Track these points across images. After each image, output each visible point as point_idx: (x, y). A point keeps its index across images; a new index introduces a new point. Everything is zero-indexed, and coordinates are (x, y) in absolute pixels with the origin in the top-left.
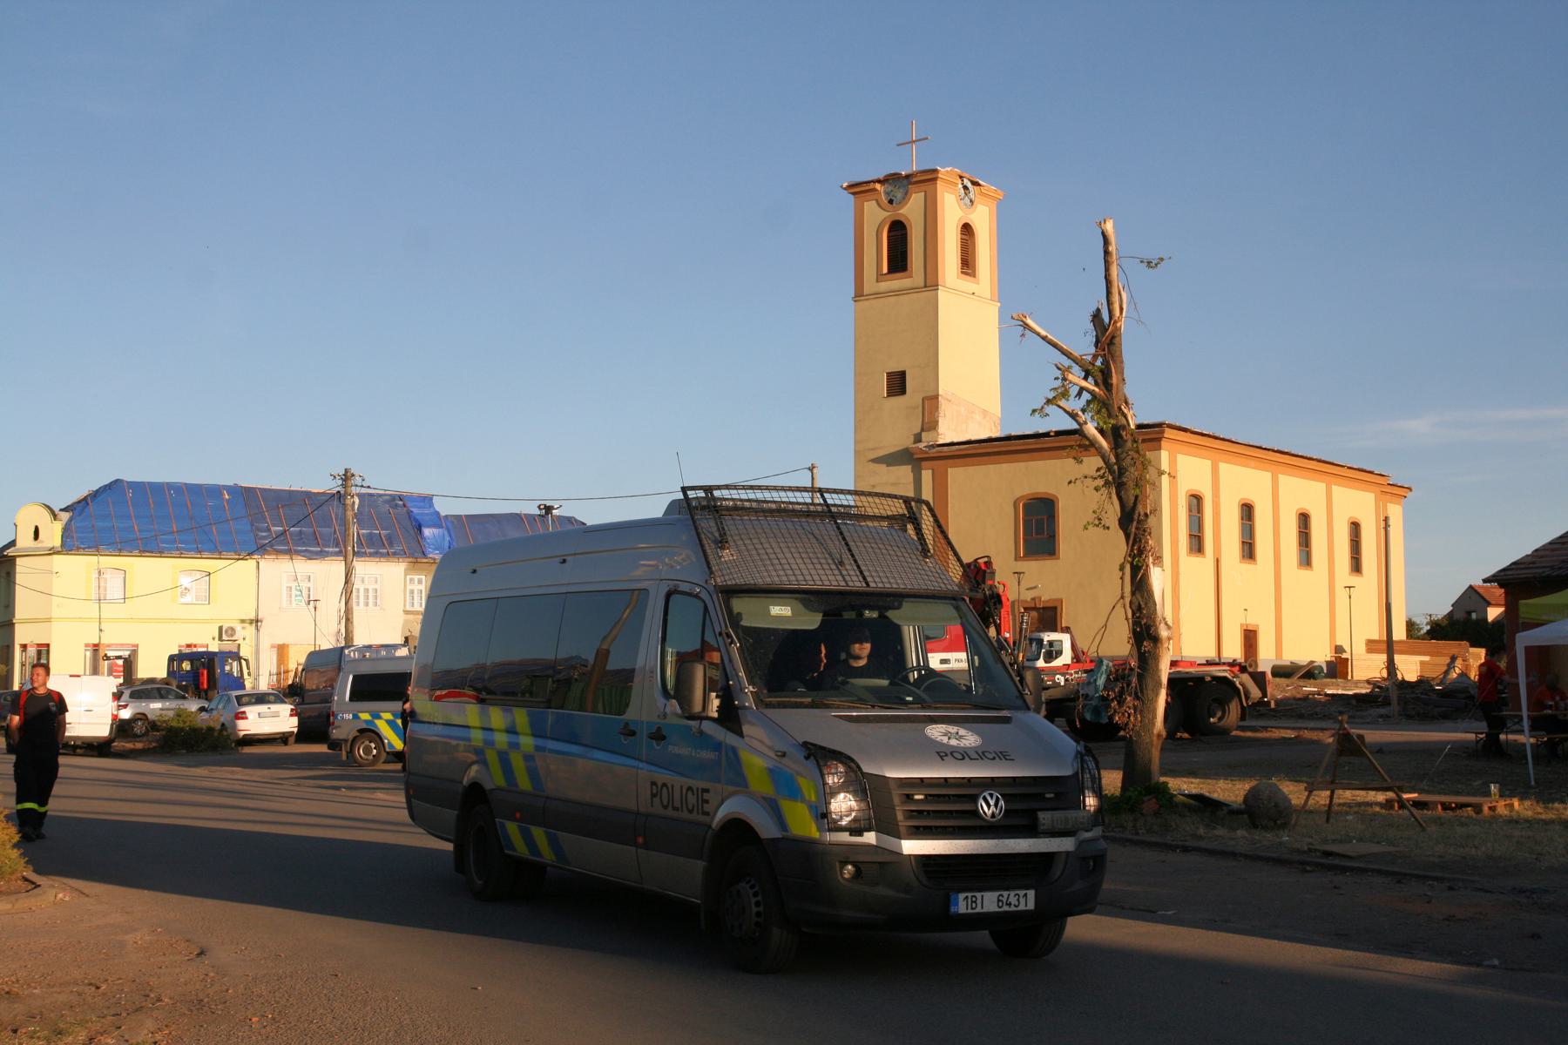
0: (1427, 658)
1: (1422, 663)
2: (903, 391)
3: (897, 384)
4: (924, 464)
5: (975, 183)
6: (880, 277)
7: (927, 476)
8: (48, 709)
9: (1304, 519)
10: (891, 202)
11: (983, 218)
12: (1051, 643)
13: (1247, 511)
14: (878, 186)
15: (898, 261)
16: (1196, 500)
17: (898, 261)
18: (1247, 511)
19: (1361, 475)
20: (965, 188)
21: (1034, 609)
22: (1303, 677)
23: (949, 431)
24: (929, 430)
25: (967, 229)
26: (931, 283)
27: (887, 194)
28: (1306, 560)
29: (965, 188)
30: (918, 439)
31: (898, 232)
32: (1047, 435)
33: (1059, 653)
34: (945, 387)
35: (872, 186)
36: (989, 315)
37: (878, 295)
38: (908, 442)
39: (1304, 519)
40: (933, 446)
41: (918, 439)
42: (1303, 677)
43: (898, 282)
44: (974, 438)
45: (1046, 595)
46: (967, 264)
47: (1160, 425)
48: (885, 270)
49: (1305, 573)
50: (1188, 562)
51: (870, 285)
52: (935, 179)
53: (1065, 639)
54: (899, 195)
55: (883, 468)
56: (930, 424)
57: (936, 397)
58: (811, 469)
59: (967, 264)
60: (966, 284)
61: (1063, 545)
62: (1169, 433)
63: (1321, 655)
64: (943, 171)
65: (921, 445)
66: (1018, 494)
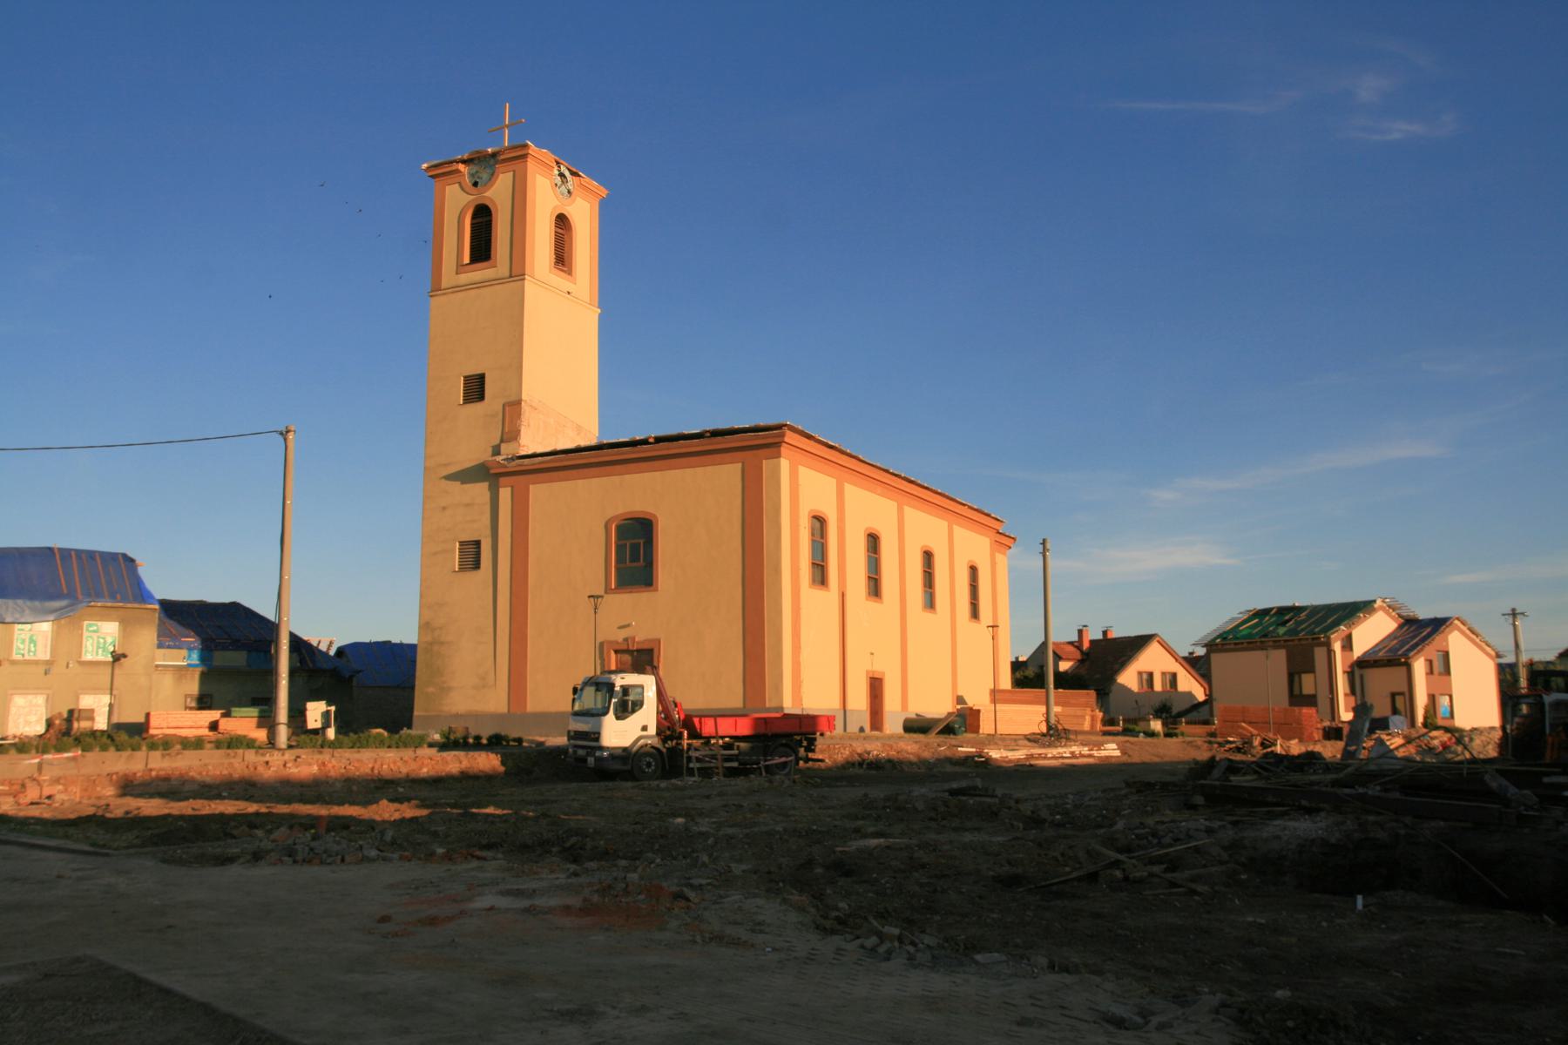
2: (481, 397)
3: (475, 388)
4: (502, 480)
5: (573, 174)
6: (460, 269)
7: (505, 494)
9: (928, 556)
10: (475, 184)
11: (584, 215)
12: (626, 690)
13: (873, 541)
14: (461, 167)
15: (481, 250)
16: (819, 521)
17: (481, 250)
18: (873, 541)
19: (980, 518)
20: (562, 175)
21: (627, 651)
22: (942, 732)
23: (534, 439)
24: (509, 441)
25: (562, 221)
26: (517, 274)
27: (472, 175)
28: (930, 604)
29: (562, 175)
31: (483, 217)
32: (645, 442)
33: (638, 705)
34: (531, 390)
35: (454, 167)
37: (458, 288)
38: (484, 455)
39: (928, 556)
40: (512, 459)
42: (942, 732)
43: (482, 273)
44: (560, 447)
45: (641, 634)
46: (562, 258)
47: (779, 427)
48: (467, 260)
49: (929, 615)
51: (449, 277)
52: (525, 156)
53: (648, 682)
54: (485, 176)
55: (456, 486)
56: (511, 435)
57: (519, 402)
58: (284, 434)
59: (562, 258)
62: (790, 437)
63: (938, 707)
65: (499, 458)
66: (611, 513)
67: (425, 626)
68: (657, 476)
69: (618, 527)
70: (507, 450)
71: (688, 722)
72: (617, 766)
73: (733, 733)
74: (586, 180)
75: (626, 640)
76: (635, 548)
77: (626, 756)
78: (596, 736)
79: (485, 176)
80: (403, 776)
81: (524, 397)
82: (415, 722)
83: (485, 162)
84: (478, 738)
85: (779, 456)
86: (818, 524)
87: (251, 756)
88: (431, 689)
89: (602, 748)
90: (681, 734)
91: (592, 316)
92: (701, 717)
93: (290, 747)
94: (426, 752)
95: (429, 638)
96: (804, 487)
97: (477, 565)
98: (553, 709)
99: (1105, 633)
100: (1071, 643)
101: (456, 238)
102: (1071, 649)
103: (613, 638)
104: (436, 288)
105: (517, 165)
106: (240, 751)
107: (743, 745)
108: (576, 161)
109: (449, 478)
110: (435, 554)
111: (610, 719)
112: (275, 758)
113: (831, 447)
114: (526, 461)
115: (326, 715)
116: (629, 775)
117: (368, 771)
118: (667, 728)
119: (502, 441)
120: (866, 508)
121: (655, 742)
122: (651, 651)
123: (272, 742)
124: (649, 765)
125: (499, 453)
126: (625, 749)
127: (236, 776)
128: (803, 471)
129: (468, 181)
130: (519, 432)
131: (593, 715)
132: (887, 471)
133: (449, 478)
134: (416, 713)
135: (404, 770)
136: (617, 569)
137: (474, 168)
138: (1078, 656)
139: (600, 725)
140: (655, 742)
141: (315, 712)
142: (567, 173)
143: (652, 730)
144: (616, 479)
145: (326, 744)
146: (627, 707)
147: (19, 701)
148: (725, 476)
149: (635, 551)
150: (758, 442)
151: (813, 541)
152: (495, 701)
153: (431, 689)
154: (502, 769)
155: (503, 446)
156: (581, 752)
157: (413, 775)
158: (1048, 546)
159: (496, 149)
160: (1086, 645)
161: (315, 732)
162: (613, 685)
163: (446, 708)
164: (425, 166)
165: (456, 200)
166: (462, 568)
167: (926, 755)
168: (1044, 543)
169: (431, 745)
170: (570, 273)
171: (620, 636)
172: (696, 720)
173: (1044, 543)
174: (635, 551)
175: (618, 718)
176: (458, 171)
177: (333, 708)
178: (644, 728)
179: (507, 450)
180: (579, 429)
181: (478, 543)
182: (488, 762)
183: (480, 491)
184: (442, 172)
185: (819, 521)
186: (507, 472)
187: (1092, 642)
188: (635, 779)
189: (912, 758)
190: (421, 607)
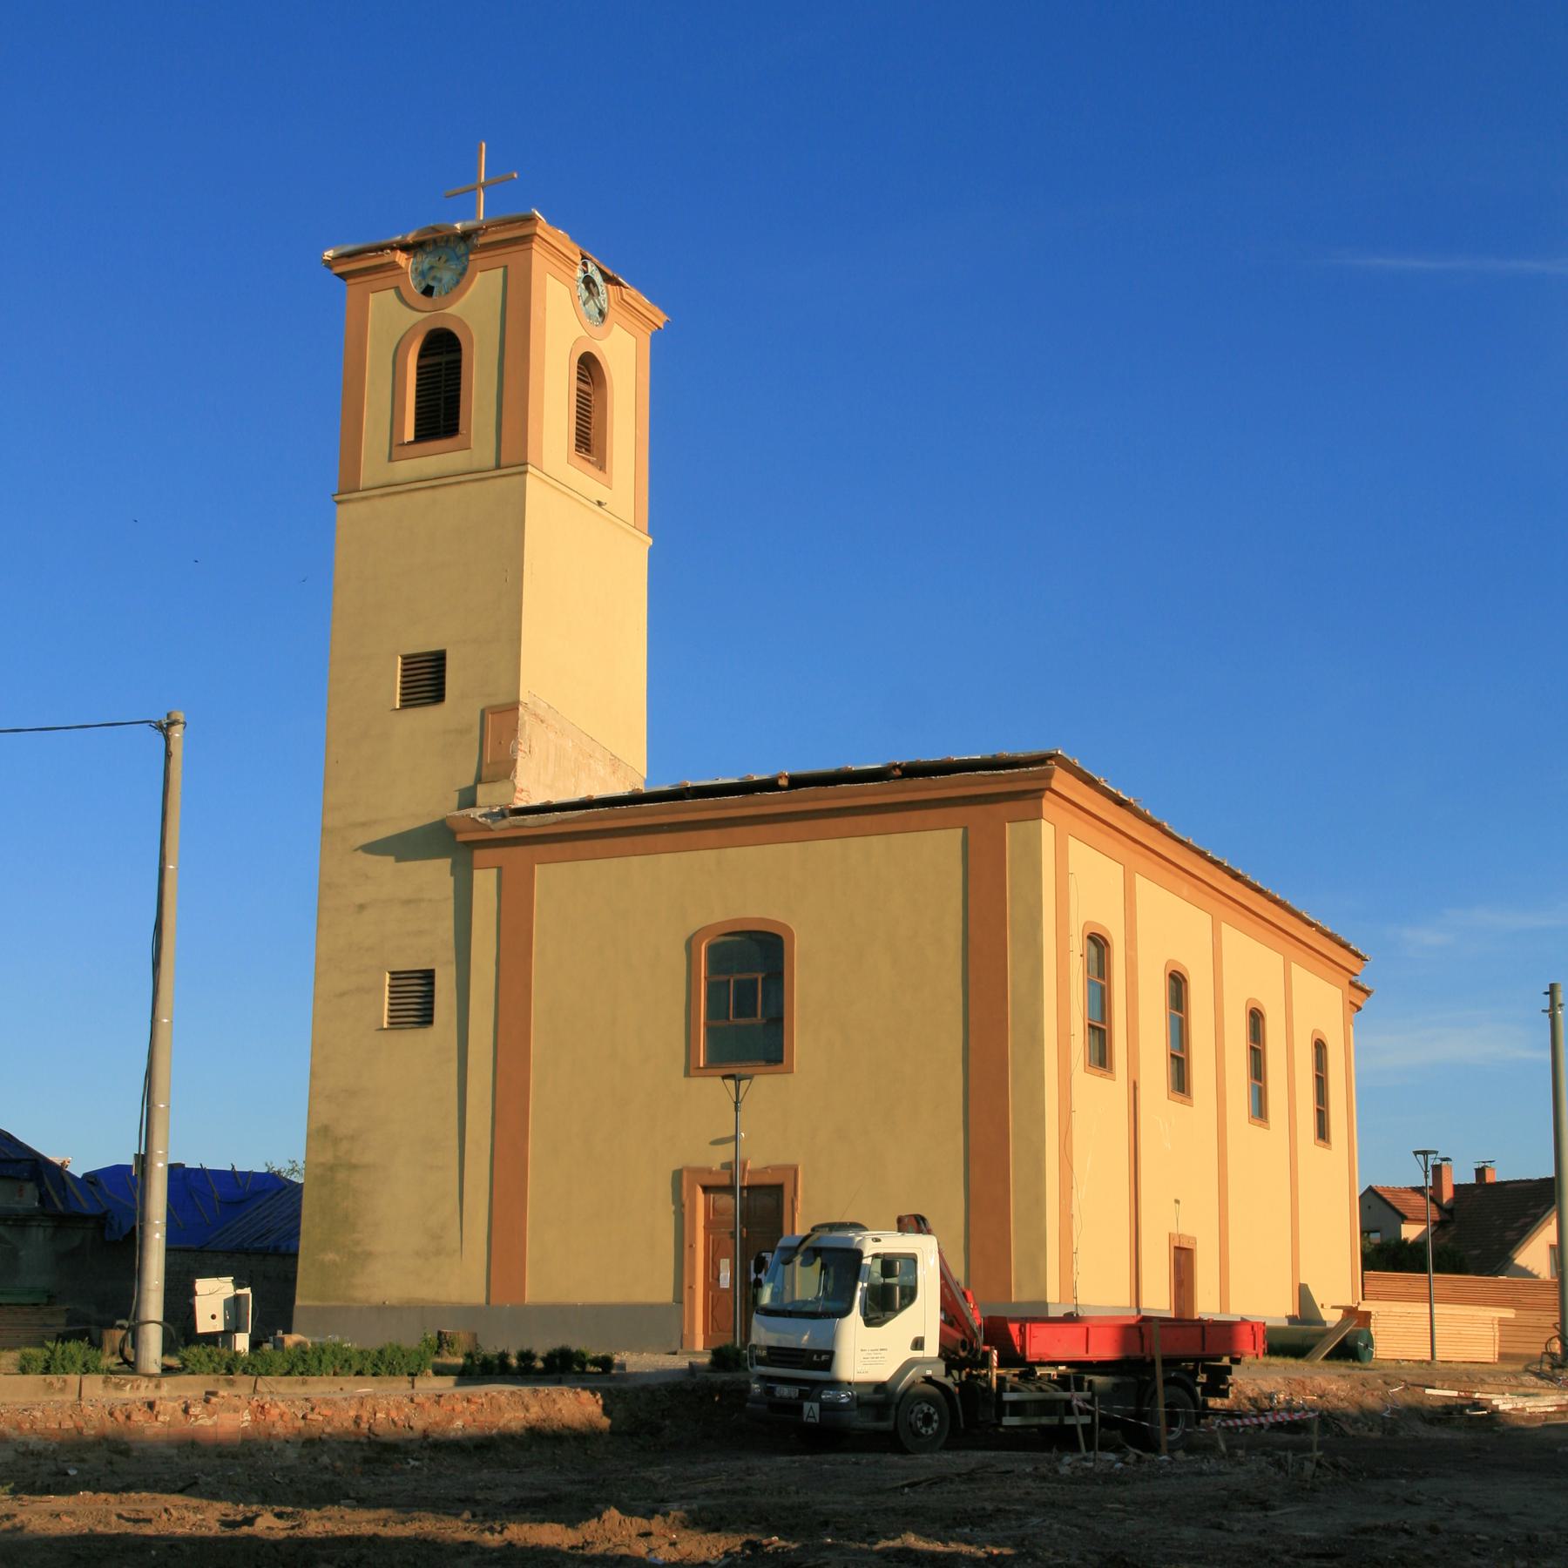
0: (1509, 1313)
1: (1503, 1323)
2: (438, 695)
3: (426, 679)
4: (479, 855)
5: (608, 279)
6: (396, 449)
7: (485, 882)
8: (748, 1389)
9: (1256, 1018)
10: (428, 291)
11: (625, 356)
12: (887, 1263)
14: (401, 258)
15: (439, 414)
16: (1098, 942)
17: (439, 414)
19: (1336, 951)
21: (729, 1189)
23: (540, 779)
25: (589, 368)
26: (511, 460)
27: (422, 275)
28: (1260, 1111)
30: (468, 799)
31: (442, 357)
32: (770, 785)
34: (537, 683)
35: (387, 256)
36: (624, 561)
37: (391, 488)
38: (445, 807)
40: (502, 815)
41: (468, 799)
43: (439, 459)
44: (598, 793)
47: (1041, 760)
48: (409, 435)
50: (1086, 1082)
51: (373, 464)
52: (527, 239)
54: (447, 277)
57: (513, 707)
58: (165, 729)
60: (580, 476)
61: (802, 1038)
62: (1062, 781)
64: (543, 227)
65: (475, 813)
66: (698, 921)
67: (320, 1134)
68: (792, 851)
69: (712, 949)
70: (491, 798)
71: (996, 1330)
72: (862, 1421)
73: (1079, 1354)
74: (631, 294)
75: (727, 1166)
76: (745, 996)
77: (880, 1397)
78: (825, 1359)
79: (447, 277)
80: (416, 1434)
81: (523, 697)
82: (298, 1318)
83: (447, 249)
84: (526, 1357)
85: (1038, 816)
86: (1094, 950)
87: (1227, 1478)
88: (330, 1256)
89: (836, 1384)
90: (986, 1355)
91: (635, 552)
92: (1023, 1321)
93: (167, 1370)
94: (430, 1384)
95: (327, 1157)
96: (1079, 876)
97: (426, 1017)
98: (579, 1297)
99: (1480, 1172)
100: (1419, 1190)
101: (388, 392)
102: (1418, 1200)
103: (699, 1162)
104: (349, 487)
105: (511, 256)
106: (73, 1379)
107: (1098, 1380)
108: (612, 264)
109: (372, 848)
110: (342, 995)
111: (853, 1322)
112: (134, 1392)
113: (1121, 803)
114: (530, 819)
115: (234, 1305)
116: (891, 1442)
117: (349, 1424)
118: (965, 1341)
119: (479, 780)
120: (1169, 925)
121: (937, 1371)
122: (777, 1189)
123: (131, 1366)
124: (927, 1420)
125: (473, 804)
126: (880, 1387)
127: (89, 1432)
128: (1078, 851)
129: (413, 285)
130: (512, 764)
131: (813, 1315)
132: (1202, 854)
133: (372, 848)
134: (298, 1302)
135: (419, 1423)
136: (710, 1030)
137: (426, 261)
138: (1433, 1213)
139: (833, 1337)
140: (937, 1371)
141: (213, 1298)
142: (598, 278)
143: (932, 1349)
144: (709, 856)
145: (231, 1366)
146: (885, 1303)
147: (202, 1285)
148: (931, 852)
149: (746, 998)
150: (988, 791)
151: (1090, 981)
152: (461, 1281)
153: (330, 1256)
154: (605, 1422)
155: (481, 790)
156: (784, 1391)
157: (435, 1435)
158: (1560, 998)
159: (470, 224)
160: (1447, 1194)
161: (211, 1338)
162: (859, 1254)
163: (359, 1294)
164: (329, 254)
165: (389, 322)
166: (396, 1023)
167: (1371, 1401)
168: (1552, 991)
169: (440, 1371)
170: (602, 468)
171: (718, 1157)
172: (1014, 1328)
173: (1552, 991)
174: (746, 998)
175: (869, 1322)
176: (394, 266)
177: (247, 1291)
178: (918, 1344)
179: (491, 798)
180: (615, 762)
181: (428, 976)
182: (576, 1406)
183: (435, 874)
184: (361, 265)
185: (1098, 942)
186: (485, 839)
187: (1457, 1188)
188: (902, 1450)
189: (1353, 1411)
190: (312, 1097)
